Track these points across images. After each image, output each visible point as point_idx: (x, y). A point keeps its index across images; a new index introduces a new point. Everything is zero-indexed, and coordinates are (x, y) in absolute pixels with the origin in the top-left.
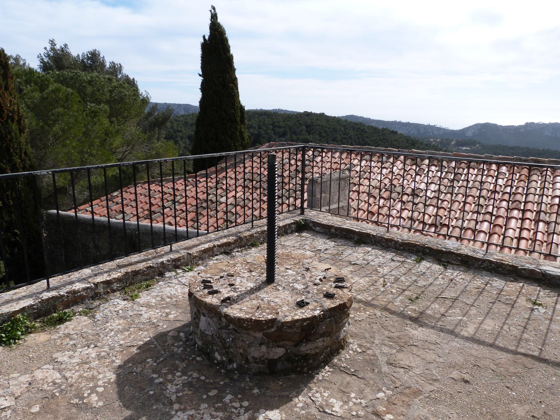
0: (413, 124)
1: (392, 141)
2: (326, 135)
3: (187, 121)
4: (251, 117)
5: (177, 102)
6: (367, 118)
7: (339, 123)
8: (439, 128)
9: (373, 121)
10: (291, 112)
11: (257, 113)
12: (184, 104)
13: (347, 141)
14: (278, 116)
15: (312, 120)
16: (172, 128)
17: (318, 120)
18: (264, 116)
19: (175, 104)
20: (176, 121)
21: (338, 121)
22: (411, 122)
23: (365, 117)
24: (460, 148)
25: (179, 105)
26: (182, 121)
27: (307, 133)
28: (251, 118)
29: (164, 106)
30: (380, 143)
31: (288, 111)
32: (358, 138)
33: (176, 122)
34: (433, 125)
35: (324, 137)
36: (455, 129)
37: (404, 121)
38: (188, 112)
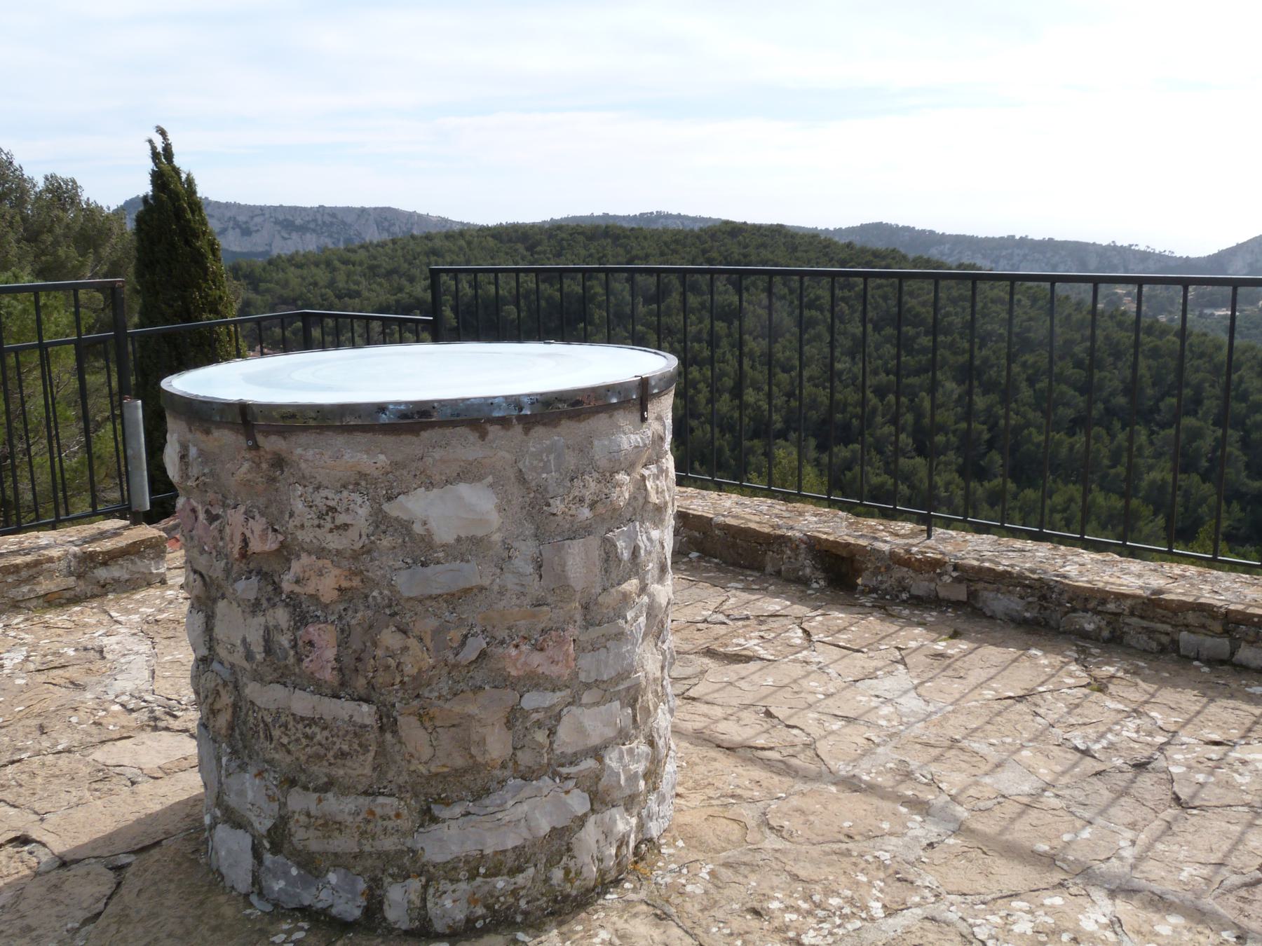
0: (1064, 245)
1: (985, 304)
2: (786, 291)
3: (375, 263)
4: (565, 243)
5: (357, 203)
6: (924, 231)
7: (826, 255)
8: (1145, 252)
9: (942, 239)
10: (695, 219)
11: (582, 233)
12: (376, 209)
13: (851, 307)
14: (645, 238)
15: (746, 247)
16: (331, 284)
17: (764, 245)
18: (604, 242)
19: (348, 210)
20: (346, 262)
21: (826, 247)
22: (1059, 237)
23: (919, 227)
24: (1208, 311)
25: (363, 211)
26: (361, 264)
27: (730, 287)
28: (562, 248)
29: (319, 217)
30: (951, 309)
31: (686, 217)
32: (885, 298)
33: (343, 267)
34: (1126, 244)
35: (783, 297)
36: (1193, 255)
37: (1037, 235)
38: (388, 231)
